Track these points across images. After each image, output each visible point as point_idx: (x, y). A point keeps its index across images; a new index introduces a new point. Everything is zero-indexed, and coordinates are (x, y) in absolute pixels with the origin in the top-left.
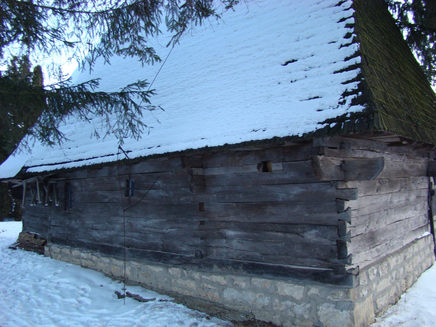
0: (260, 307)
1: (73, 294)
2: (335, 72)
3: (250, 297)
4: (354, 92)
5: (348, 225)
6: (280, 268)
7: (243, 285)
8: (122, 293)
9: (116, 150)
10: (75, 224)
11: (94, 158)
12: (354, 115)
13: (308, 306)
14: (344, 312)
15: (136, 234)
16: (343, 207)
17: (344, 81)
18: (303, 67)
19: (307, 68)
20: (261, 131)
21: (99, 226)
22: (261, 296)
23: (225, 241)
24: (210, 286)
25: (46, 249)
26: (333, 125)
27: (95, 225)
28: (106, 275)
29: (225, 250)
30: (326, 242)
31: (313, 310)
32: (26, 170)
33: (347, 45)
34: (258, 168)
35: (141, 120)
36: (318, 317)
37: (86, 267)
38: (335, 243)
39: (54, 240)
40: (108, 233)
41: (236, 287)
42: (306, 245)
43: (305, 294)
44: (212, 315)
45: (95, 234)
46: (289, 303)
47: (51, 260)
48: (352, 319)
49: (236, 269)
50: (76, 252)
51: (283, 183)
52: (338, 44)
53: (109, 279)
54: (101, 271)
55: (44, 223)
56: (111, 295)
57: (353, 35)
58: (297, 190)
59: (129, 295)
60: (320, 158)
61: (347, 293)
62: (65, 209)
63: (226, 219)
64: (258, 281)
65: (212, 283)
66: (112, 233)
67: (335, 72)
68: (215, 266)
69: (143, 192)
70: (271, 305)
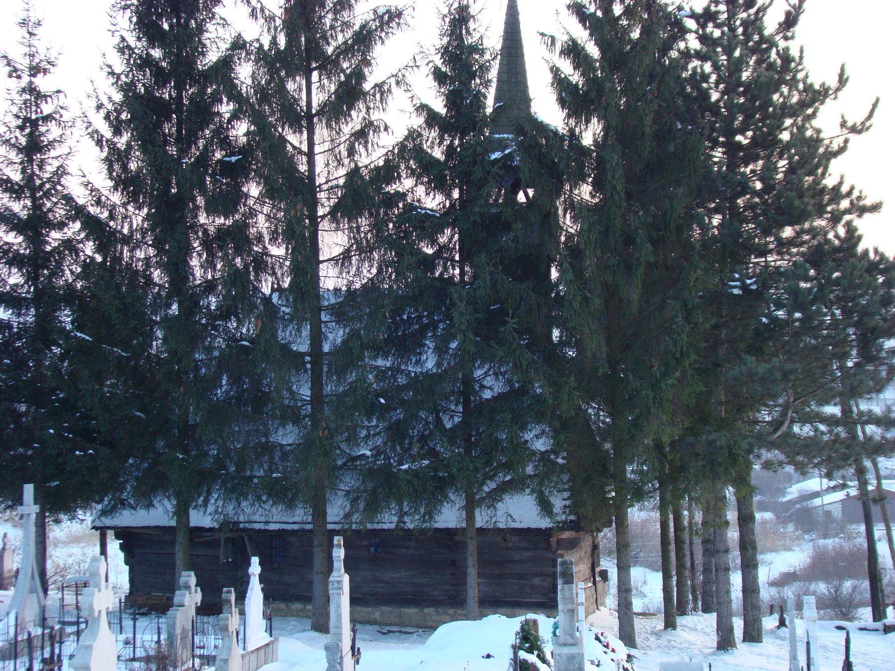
30: (545, 584)
58: (528, 554)
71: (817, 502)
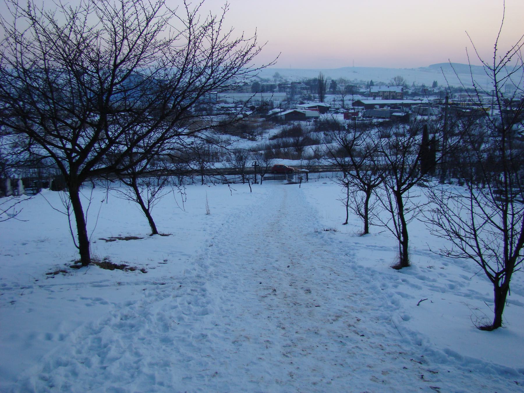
71: (279, 114)
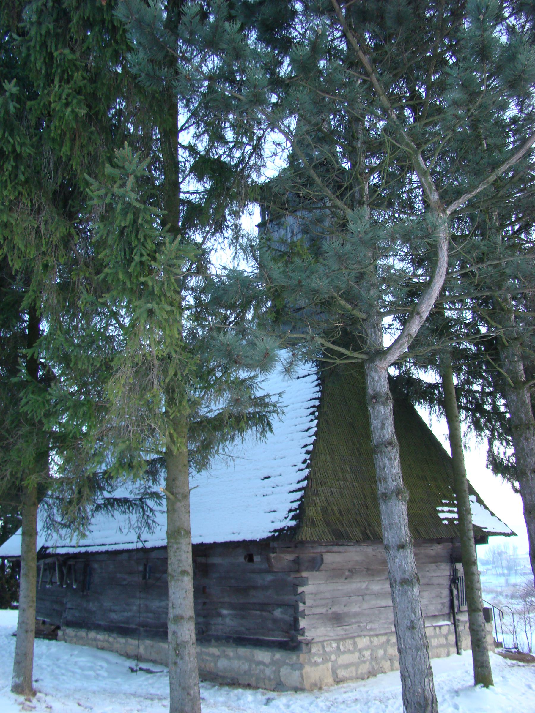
0: (242, 672)
1: (91, 668)
2: (290, 492)
3: (236, 664)
4: (296, 510)
5: (301, 605)
6: (258, 640)
7: (231, 654)
8: (135, 668)
9: (135, 539)
10: (92, 606)
11: (116, 544)
12: (290, 528)
13: (274, 668)
14: (297, 672)
15: (151, 615)
16: (297, 591)
17: (292, 500)
18: (273, 485)
19: (275, 485)
20: (236, 534)
21: (116, 608)
22: (243, 663)
23: (220, 619)
24: (208, 658)
25: (60, 633)
26: (277, 534)
27: (112, 607)
28: (121, 655)
29: (221, 627)
31: (277, 672)
32: (46, 551)
33: (302, 470)
34: (245, 558)
35: (156, 520)
36: (280, 677)
37: (102, 649)
38: (292, 619)
39: (69, 624)
40: (126, 614)
41: (227, 657)
42: (275, 621)
43: (272, 659)
44: (206, 680)
45: (113, 616)
46: (262, 667)
47: (65, 644)
48: (302, 677)
49: (228, 642)
50: (92, 634)
51: (261, 571)
52: (296, 468)
53: (124, 658)
54: (117, 652)
55: (55, 607)
56: (126, 669)
57: (308, 461)
59: (141, 669)
60: (272, 555)
61: (298, 657)
62: (83, 591)
63: (222, 600)
64: (243, 651)
65: (209, 655)
66: (130, 614)
67: (290, 492)
68: (213, 641)
69: (158, 575)
70: (250, 670)
